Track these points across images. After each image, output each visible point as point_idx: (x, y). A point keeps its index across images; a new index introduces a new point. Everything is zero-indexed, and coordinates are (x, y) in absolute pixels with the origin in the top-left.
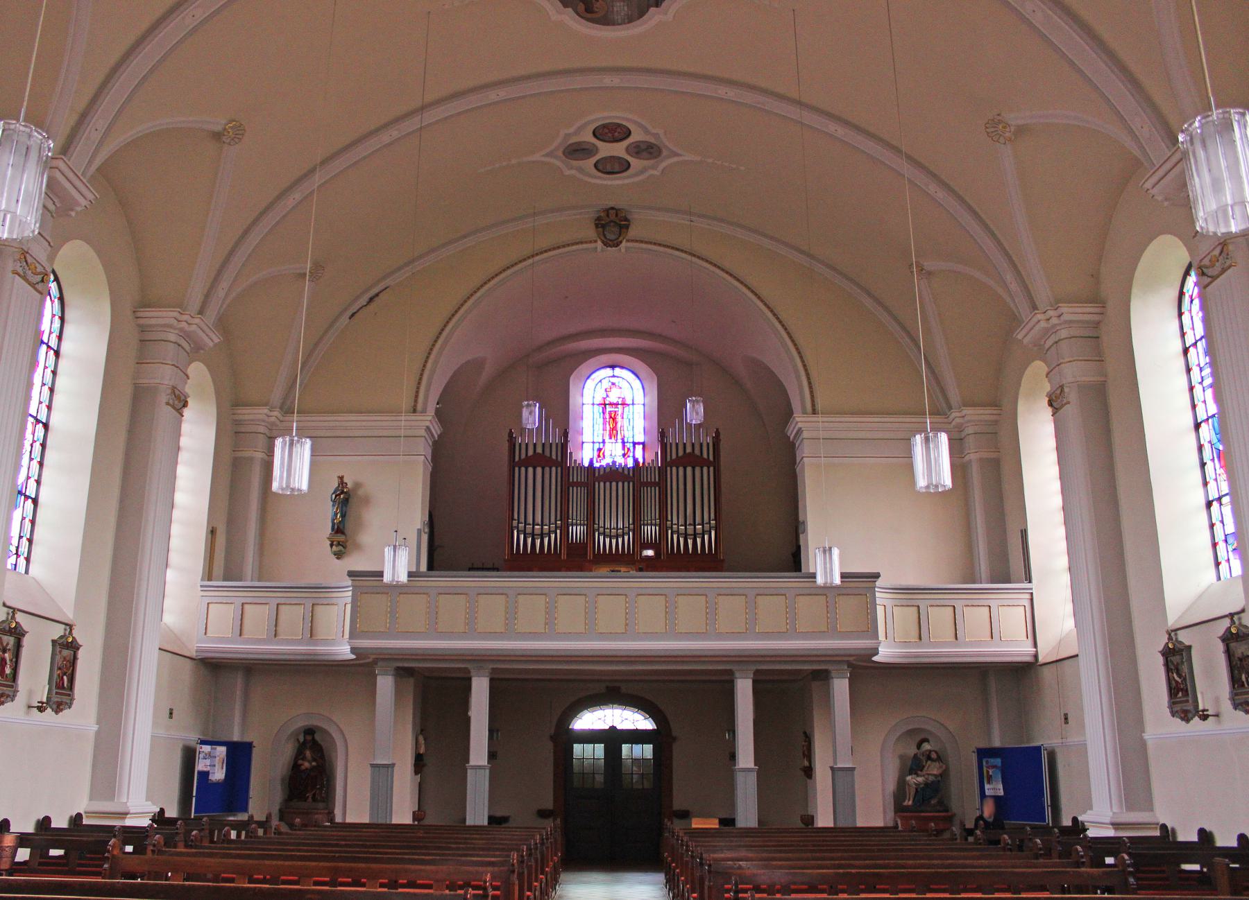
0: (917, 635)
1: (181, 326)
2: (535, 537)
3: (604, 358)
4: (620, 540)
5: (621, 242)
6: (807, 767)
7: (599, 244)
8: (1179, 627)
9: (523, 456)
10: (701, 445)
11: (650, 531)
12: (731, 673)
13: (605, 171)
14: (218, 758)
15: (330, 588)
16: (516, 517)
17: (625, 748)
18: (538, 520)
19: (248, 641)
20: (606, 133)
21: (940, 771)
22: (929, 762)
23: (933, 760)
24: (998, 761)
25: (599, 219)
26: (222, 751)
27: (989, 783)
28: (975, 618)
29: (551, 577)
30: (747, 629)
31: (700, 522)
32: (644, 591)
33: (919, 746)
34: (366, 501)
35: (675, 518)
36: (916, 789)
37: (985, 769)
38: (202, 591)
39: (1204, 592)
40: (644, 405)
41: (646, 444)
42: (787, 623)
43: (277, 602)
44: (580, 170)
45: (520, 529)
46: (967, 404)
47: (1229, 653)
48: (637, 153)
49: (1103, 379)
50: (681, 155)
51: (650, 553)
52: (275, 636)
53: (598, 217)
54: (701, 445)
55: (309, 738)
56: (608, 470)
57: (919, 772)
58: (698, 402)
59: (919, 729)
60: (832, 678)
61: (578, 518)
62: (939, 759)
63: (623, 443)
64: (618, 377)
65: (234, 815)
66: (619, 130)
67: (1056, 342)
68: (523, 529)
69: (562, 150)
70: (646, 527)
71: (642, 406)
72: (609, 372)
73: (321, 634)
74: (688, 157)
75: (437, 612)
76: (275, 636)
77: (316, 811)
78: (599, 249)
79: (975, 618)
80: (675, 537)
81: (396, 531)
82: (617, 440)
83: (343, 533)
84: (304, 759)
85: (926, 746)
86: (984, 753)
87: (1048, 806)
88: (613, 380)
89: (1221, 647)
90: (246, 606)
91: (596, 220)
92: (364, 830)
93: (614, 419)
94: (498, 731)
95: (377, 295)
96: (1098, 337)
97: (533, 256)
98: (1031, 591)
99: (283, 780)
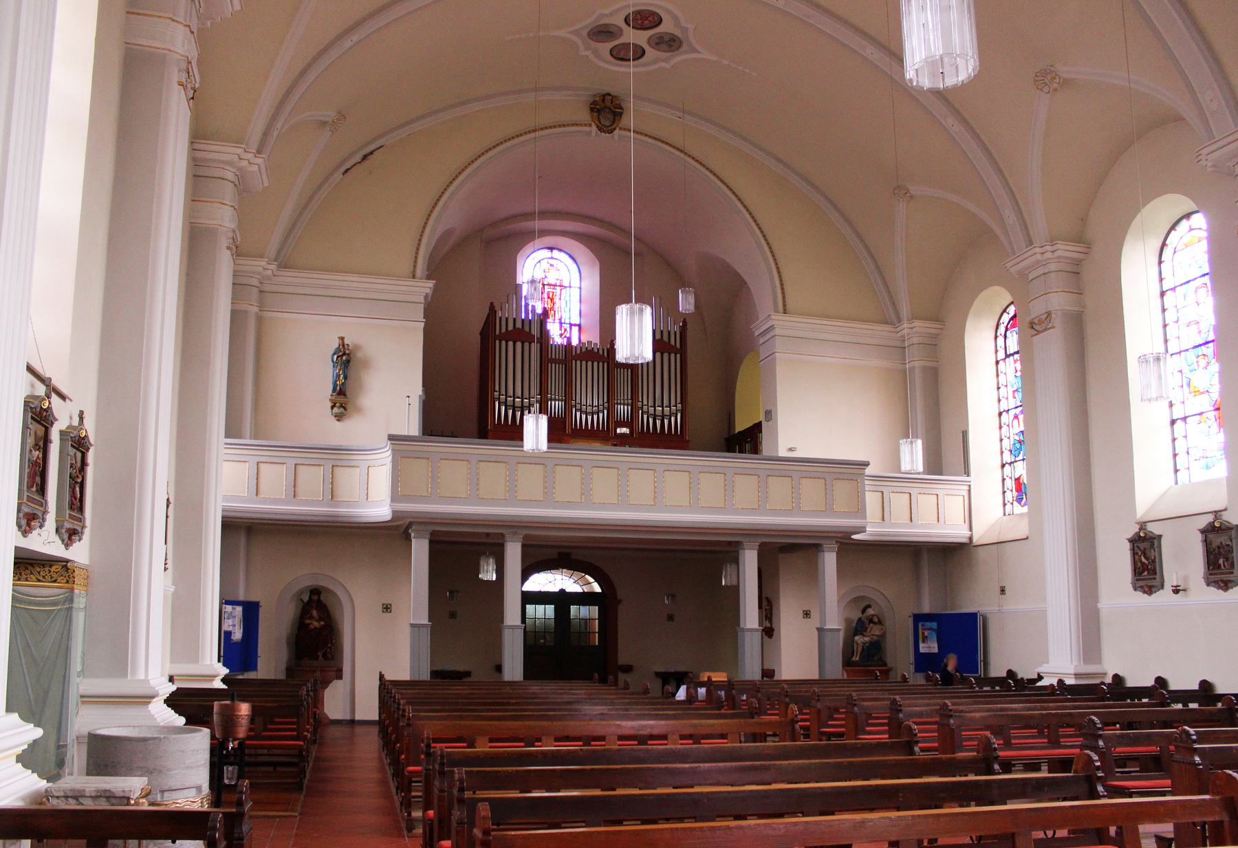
0: (881, 517)
1: (240, 165)
2: (516, 409)
3: (549, 240)
4: (595, 417)
5: (615, 129)
6: (769, 628)
7: (594, 128)
8: (1147, 520)
9: (504, 330)
10: (669, 332)
11: (623, 410)
12: (502, 535)
13: (618, 56)
14: (237, 618)
15: (352, 450)
16: (497, 388)
17: (573, 609)
18: (519, 393)
19: (265, 501)
20: (637, 20)
21: (882, 632)
22: (871, 625)
23: (874, 623)
24: (934, 625)
25: (594, 103)
26: (239, 609)
27: (924, 642)
28: (925, 503)
29: (710, 457)
30: (759, 506)
31: (668, 405)
32: (706, 469)
33: (864, 611)
34: (366, 364)
35: (645, 400)
36: (863, 647)
37: (920, 631)
38: (226, 444)
39: (1164, 493)
40: (580, 288)
41: (582, 326)
42: (793, 502)
43: (257, 461)
44: (595, 52)
45: (644, 410)
46: (914, 317)
47: (1206, 542)
48: (657, 44)
49: (1081, 310)
50: (700, 52)
51: (625, 430)
52: (294, 496)
53: (594, 102)
54: (669, 332)
55: (315, 598)
56: (584, 350)
57: (864, 633)
58: (689, 292)
59: (863, 597)
60: (823, 551)
61: (560, 395)
62: (880, 622)
63: (561, 323)
64: (556, 259)
65: (243, 674)
66: (650, 19)
67: (1045, 274)
68: (512, 404)
69: (588, 30)
70: (553, 403)
71: (579, 290)
72: (545, 253)
73: (342, 495)
74: (706, 55)
75: (478, 479)
76: (294, 496)
77: (328, 669)
78: (593, 134)
79: (925, 503)
80: (645, 416)
81: (409, 397)
82: (554, 320)
83: (345, 395)
84: (311, 617)
85: (870, 612)
86: (919, 618)
87: (981, 661)
88: (552, 262)
89: (1199, 537)
90: (262, 465)
91: (591, 104)
92: (454, 688)
93: (552, 300)
94: (457, 592)
95: (371, 153)
96: (1078, 273)
97: (534, 131)
98: (969, 484)
99: (288, 639)
